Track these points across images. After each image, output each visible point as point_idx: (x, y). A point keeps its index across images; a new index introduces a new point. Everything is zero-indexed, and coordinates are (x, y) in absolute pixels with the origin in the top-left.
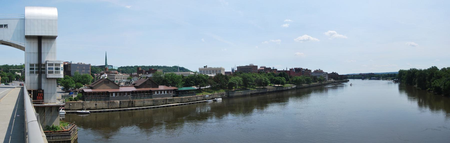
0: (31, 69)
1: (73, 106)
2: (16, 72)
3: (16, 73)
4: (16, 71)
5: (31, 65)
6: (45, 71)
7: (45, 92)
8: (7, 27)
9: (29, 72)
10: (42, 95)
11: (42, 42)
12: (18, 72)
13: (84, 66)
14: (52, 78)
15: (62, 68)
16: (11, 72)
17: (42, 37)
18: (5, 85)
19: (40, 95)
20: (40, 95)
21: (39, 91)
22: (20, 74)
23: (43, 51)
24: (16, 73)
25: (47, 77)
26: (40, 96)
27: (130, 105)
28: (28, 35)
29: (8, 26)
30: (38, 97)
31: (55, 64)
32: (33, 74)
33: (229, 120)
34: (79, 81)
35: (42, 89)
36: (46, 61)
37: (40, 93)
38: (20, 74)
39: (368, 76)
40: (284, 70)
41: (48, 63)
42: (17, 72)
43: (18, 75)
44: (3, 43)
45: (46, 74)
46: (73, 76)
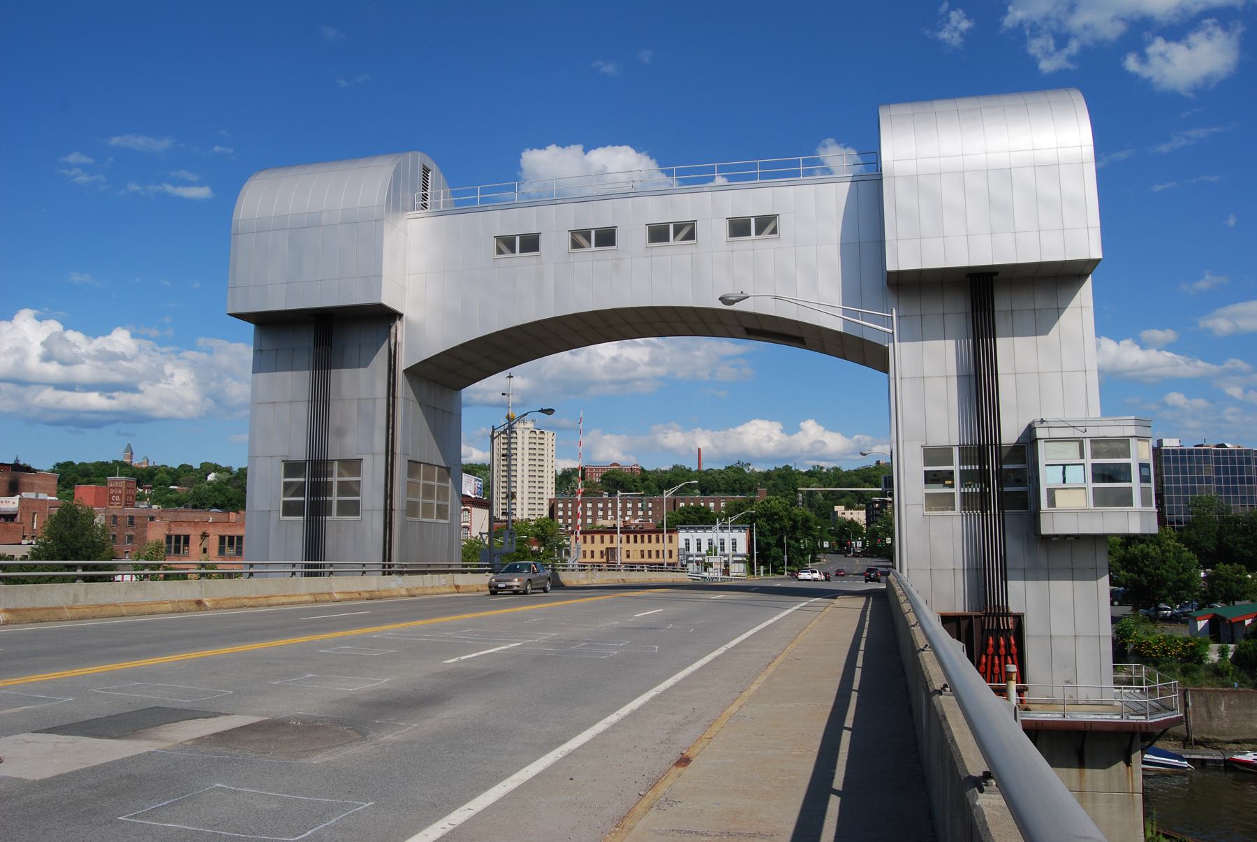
0: (931, 478)
1: (1210, 717)
2: (837, 508)
3: (839, 509)
4: (838, 498)
5: (933, 454)
6: (1025, 492)
7: (1031, 628)
8: (774, 231)
9: (922, 500)
10: (1014, 650)
11: (996, 308)
12: (849, 507)
13: (1207, 460)
14: (1078, 537)
15: (1147, 466)
16: (810, 506)
17: (996, 274)
18: (866, 581)
19: (1002, 651)
20: (1002, 651)
21: (990, 624)
22: (860, 516)
23: (335, 420)
24: (839, 509)
25: (1046, 529)
26: (997, 652)
27: (1119, 669)
28: (902, 268)
29: (783, 224)
30: (984, 660)
31: (1094, 441)
32: (950, 513)
33: (136, 567)
34: (1228, 555)
35: (1014, 608)
36: (1031, 429)
37: (999, 632)
38: (860, 516)
39: (95, 479)
40: (878, 462)
41: (1040, 433)
42: (842, 508)
43: (852, 523)
44: (753, 325)
45: (1032, 507)
46: (1179, 522)
